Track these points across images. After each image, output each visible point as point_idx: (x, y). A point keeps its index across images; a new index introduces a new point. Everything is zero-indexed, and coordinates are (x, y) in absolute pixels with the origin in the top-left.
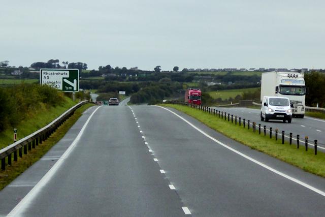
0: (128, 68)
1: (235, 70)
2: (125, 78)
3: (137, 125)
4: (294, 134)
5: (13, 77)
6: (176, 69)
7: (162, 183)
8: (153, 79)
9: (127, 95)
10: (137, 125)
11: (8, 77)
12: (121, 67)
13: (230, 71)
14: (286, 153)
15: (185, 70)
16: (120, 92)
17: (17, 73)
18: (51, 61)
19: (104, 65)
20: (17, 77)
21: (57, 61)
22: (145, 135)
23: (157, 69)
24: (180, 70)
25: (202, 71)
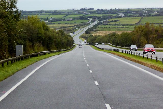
6: (116, 9)
15: (118, 9)
18: (85, 8)
23: (111, 9)
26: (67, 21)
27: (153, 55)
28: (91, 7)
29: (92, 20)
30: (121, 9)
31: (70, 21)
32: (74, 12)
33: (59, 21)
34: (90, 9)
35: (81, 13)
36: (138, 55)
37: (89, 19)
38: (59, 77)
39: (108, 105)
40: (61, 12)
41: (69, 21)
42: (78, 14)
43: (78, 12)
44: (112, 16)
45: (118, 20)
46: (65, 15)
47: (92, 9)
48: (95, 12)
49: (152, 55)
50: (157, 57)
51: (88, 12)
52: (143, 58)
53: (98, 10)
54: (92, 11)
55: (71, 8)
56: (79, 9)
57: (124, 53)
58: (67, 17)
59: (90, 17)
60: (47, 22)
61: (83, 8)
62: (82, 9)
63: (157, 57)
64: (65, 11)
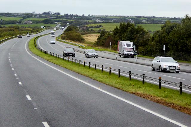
0: (74, 15)
1: (108, 16)
2: (71, 18)
3: (10, 64)
4: (54, 54)
5: (36, 17)
6: (89, 15)
7: (11, 68)
8: (80, 19)
9: (69, 24)
10: (10, 64)
11: (35, 17)
12: (71, 14)
13: (106, 16)
14: (46, 57)
15: (92, 16)
16: (67, 24)
17: (38, 16)
18: (49, 12)
19: (66, 13)
20: (38, 18)
21: (51, 12)
22: (12, 64)
23: (83, 15)
24: (91, 15)
25: (97, 16)
26: (25, 24)
27: (74, 58)
28: (57, 12)
29: (60, 24)
30: (96, 16)
31: (28, 24)
32: (33, 15)
33: (13, 23)
34: (56, 13)
35: (44, 17)
36: (93, 66)
37: (56, 24)
38: (27, 118)
39: (45, 124)
40: (17, 15)
41: (27, 24)
42: (40, 18)
43: (40, 16)
44: (88, 21)
45: (100, 26)
46: (22, 18)
47: (58, 14)
48: (62, 16)
49: (72, 58)
50: (90, 63)
51: (53, 16)
52: (142, 83)
53: (67, 15)
54: (59, 15)
55: (30, 11)
56: (41, 13)
57: (57, 57)
58: (24, 20)
59: (58, 21)
60: (145, 21)
61: (47, 12)
62: (45, 13)
63: (120, 69)
64: (23, 14)
